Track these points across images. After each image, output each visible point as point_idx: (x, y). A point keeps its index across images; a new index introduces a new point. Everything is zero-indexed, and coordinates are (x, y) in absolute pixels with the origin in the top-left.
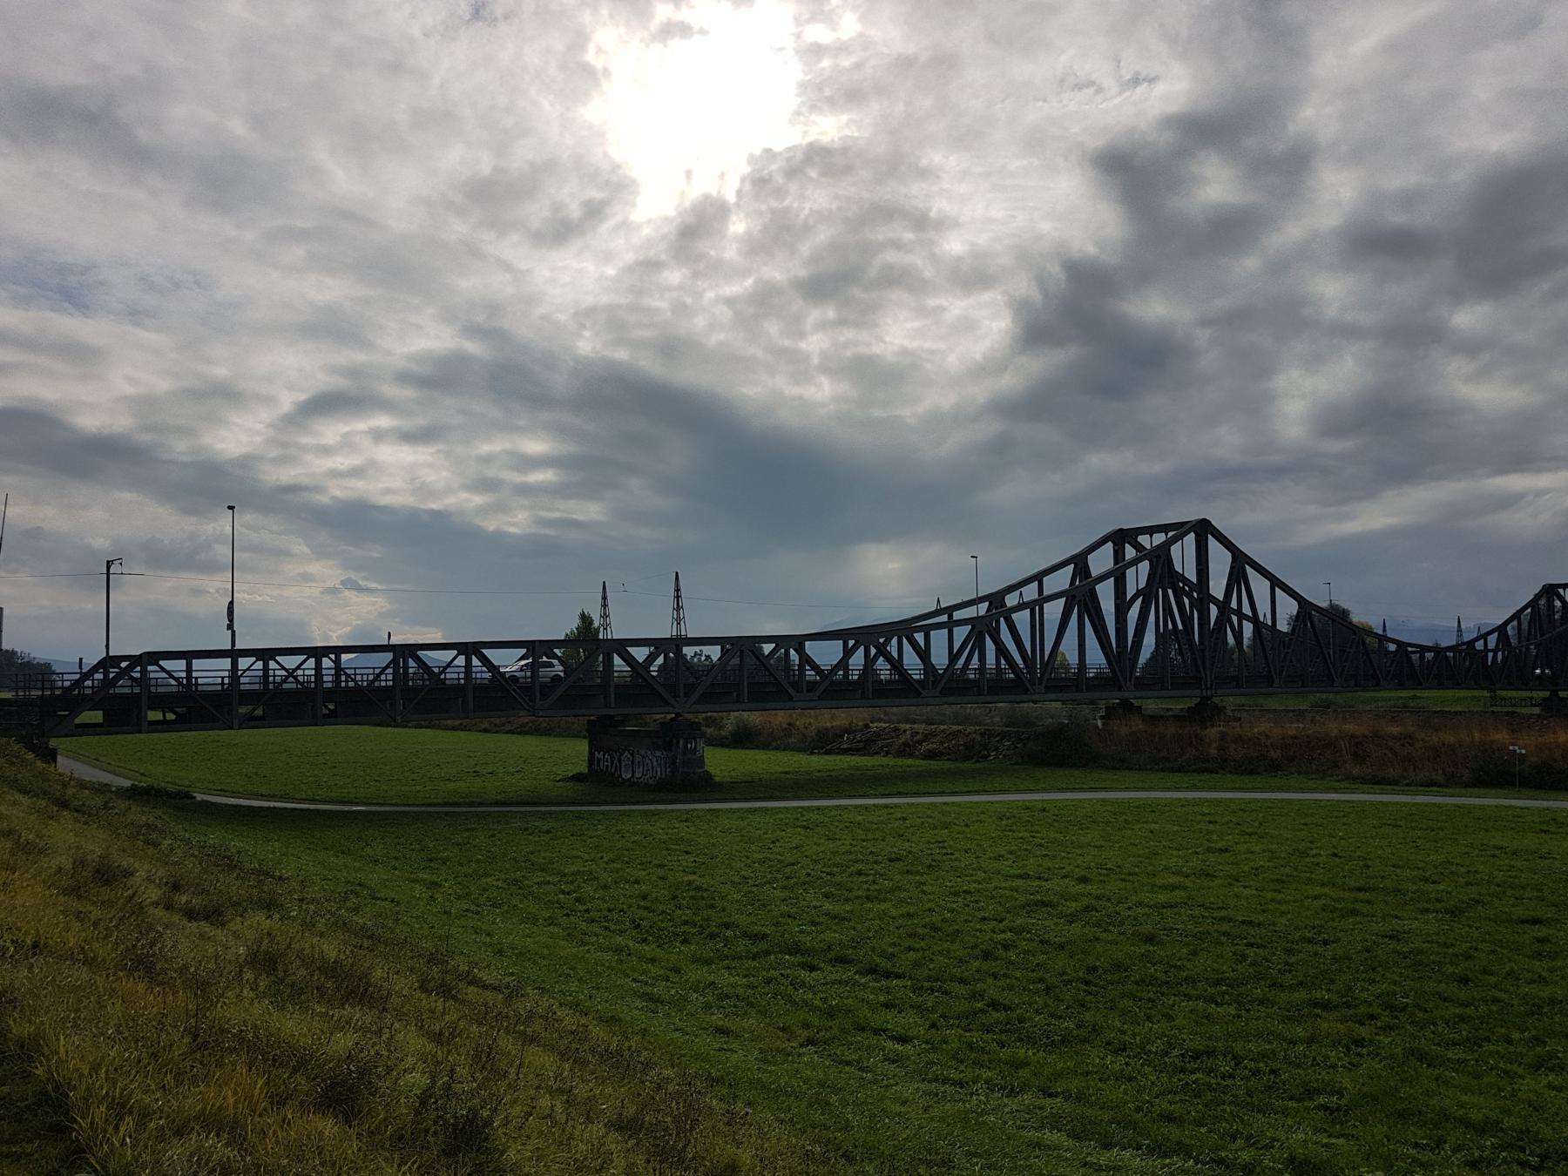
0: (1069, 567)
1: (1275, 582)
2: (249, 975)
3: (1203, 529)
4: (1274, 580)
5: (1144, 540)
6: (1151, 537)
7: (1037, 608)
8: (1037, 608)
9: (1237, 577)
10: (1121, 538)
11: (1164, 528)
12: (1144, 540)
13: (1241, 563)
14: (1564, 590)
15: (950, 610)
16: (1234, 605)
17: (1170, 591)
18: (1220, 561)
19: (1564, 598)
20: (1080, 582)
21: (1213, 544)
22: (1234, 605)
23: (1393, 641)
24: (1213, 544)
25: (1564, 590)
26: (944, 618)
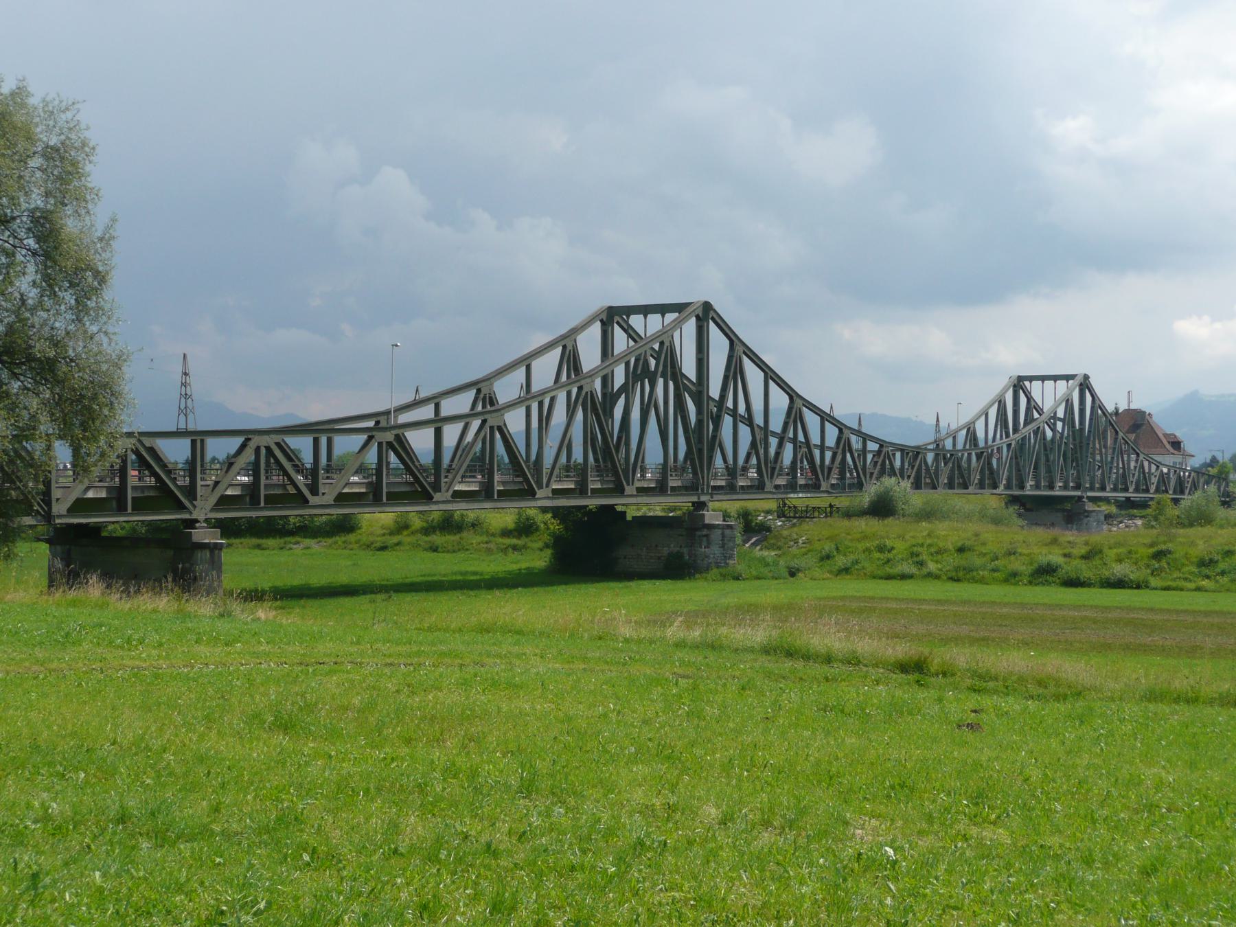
0: (556, 350)
1: (770, 375)
2: (35, 867)
3: (706, 314)
4: (770, 373)
5: (636, 321)
6: (663, 316)
7: (639, 372)
8: (639, 372)
9: (734, 372)
10: (612, 317)
11: (662, 309)
12: (636, 321)
13: (739, 351)
14: (1031, 383)
15: (435, 400)
16: (730, 404)
17: (671, 384)
18: (719, 347)
19: (1030, 393)
20: (575, 376)
21: (713, 330)
22: (730, 404)
23: (874, 439)
24: (713, 330)
25: (1031, 383)
26: (427, 412)
